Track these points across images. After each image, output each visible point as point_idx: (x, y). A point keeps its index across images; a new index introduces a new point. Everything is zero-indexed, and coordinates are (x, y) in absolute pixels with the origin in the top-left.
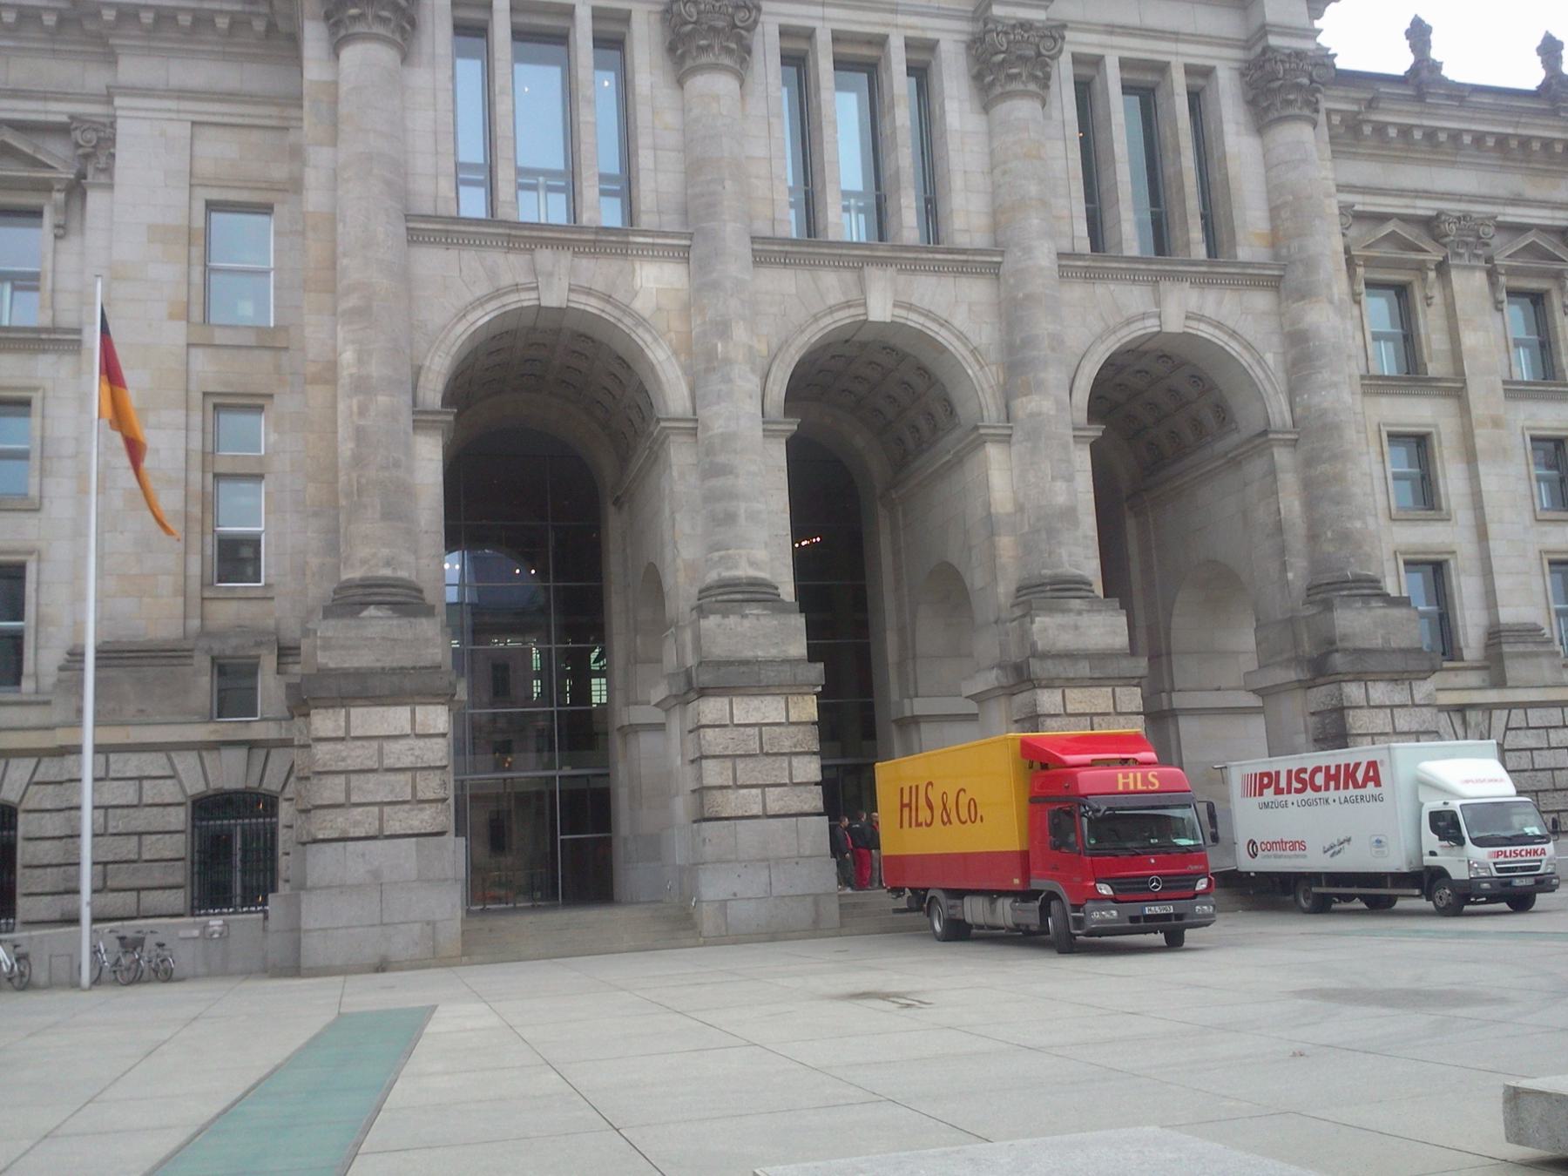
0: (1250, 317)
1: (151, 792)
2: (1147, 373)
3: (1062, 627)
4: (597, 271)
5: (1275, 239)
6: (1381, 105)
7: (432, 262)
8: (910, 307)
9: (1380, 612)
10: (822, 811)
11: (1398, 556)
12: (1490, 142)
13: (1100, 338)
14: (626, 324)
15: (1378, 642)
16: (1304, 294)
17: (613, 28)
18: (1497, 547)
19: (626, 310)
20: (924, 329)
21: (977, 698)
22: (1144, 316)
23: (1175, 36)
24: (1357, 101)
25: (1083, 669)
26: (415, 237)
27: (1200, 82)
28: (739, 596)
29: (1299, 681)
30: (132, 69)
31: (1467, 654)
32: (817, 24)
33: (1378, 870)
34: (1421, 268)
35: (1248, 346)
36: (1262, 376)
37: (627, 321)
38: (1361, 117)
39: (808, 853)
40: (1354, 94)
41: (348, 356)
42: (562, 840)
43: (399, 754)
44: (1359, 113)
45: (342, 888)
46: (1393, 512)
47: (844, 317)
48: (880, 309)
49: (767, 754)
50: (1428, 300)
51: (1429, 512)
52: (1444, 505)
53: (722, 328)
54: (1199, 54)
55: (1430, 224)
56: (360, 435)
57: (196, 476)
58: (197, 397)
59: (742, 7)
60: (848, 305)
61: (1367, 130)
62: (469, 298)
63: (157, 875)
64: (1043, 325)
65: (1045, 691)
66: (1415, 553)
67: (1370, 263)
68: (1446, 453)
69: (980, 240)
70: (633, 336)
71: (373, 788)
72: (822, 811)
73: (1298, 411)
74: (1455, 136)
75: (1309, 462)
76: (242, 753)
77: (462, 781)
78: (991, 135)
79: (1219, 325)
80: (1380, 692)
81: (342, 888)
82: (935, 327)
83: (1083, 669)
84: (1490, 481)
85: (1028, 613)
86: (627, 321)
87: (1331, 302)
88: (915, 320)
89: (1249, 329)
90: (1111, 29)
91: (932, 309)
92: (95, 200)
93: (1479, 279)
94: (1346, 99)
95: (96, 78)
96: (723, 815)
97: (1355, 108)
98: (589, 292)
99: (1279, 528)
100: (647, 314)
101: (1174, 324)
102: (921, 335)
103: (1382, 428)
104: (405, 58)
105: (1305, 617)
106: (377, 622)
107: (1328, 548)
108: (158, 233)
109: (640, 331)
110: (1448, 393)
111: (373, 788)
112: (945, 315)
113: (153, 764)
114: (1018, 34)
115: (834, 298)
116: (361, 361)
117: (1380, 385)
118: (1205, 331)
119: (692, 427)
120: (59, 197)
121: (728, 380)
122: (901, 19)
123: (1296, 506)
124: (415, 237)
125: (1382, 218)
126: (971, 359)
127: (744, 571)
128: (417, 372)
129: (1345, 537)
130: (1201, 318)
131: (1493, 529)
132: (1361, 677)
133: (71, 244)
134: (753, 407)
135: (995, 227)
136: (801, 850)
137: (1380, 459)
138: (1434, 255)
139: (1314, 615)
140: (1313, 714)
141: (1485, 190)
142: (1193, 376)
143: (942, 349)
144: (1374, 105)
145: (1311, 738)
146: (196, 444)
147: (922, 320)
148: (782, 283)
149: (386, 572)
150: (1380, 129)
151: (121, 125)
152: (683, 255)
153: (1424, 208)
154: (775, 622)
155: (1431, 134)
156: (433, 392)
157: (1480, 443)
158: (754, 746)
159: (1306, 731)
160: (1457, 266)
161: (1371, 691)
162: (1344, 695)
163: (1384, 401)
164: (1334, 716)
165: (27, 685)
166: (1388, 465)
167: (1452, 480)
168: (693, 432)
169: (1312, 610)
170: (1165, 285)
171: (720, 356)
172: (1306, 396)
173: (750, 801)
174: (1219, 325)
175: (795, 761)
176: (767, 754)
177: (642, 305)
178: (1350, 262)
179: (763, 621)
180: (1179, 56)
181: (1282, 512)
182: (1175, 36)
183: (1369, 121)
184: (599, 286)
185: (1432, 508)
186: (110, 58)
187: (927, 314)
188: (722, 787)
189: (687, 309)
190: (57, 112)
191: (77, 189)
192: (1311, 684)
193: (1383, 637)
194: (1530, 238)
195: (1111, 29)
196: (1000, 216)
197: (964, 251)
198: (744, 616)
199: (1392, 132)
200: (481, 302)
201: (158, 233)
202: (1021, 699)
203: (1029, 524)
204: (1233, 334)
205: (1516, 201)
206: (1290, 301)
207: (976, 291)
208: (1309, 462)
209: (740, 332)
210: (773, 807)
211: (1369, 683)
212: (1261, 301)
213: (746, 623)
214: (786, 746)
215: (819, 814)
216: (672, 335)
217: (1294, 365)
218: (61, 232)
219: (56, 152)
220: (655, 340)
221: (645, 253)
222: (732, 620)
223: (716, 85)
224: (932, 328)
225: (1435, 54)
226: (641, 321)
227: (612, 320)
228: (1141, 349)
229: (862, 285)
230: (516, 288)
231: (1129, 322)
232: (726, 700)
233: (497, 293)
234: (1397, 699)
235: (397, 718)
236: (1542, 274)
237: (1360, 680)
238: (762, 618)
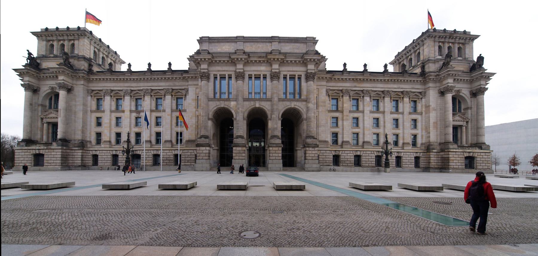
1: (192, 154)
3: (273, 141)
4: (227, 103)
5: (307, 96)
7: (211, 103)
8: (261, 105)
12: (351, 79)
13: (284, 108)
14: (230, 108)
15: (311, 143)
16: (309, 102)
17: (230, 76)
18: (345, 131)
19: (230, 107)
21: (301, 148)
22: (289, 105)
23: (297, 71)
26: (209, 101)
27: (300, 76)
30: (190, 83)
31: (339, 144)
32: (252, 74)
35: (302, 109)
40: (330, 74)
41: (201, 113)
43: (204, 152)
45: (199, 163)
47: (253, 107)
48: (257, 106)
50: (340, 100)
53: (239, 109)
54: (300, 73)
56: (202, 121)
57: (196, 124)
58: (196, 116)
59: (303, 55)
60: (254, 105)
63: (192, 161)
64: (275, 107)
67: (332, 96)
68: (340, 120)
69: (270, 97)
71: (202, 155)
74: (346, 79)
75: (307, 123)
76: (156, 151)
78: (272, 85)
79: (298, 106)
80: (311, 149)
81: (199, 163)
83: (275, 145)
84: (345, 123)
85: (306, 139)
87: (312, 103)
88: (261, 107)
89: (302, 107)
90: (288, 71)
92: (187, 96)
93: (348, 97)
94: (329, 75)
95: (187, 84)
98: (226, 105)
101: (293, 106)
104: (208, 82)
106: (203, 139)
107: (308, 132)
108: (193, 100)
110: (341, 112)
111: (202, 155)
113: (192, 151)
114: (275, 73)
115: (252, 105)
116: (202, 114)
118: (297, 107)
119: (236, 119)
120: (184, 96)
121: (239, 114)
122: (262, 72)
123: (306, 127)
124: (209, 101)
127: (239, 134)
128: (209, 114)
129: (310, 131)
130: (296, 105)
131: (344, 129)
132: (308, 147)
133: (185, 101)
134: (242, 117)
135: (272, 96)
138: (341, 95)
141: (350, 86)
146: (196, 121)
148: (247, 103)
149: (204, 134)
150: (335, 79)
151: (189, 89)
152: (236, 101)
153: (341, 88)
155: (342, 79)
156: (211, 116)
157: (344, 118)
160: (345, 96)
163: (332, 113)
165: (183, 143)
167: (340, 123)
168: (236, 119)
170: (291, 102)
173: (238, 158)
174: (298, 106)
177: (231, 106)
180: (297, 74)
182: (297, 71)
184: (227, 105)
186: (188, 81)
187: (263, 106)
189: (236, 107)
190: (183, 88)
191: (185, 96)
194: (356, 92)
195: (288, 71)
196: (272, 94)
199: (337, 79)
200: (215, 107)
201: (193, 100)
202: (305, 148)
204: (300, 107)
205: (356, 87)
207: (269, 103)
208: (307, 123)
209: (240, 109)
212: (304, 103)
214: (242, 152)
218: (185, 100)
219: (184, 92)
223: (240, 82)
224: (263, 108)
225: (347, 68)
226: (231, 108)
229: (255, 103)
230: (219, 105)
231: (287, 106)
233: (217, 106)
234: (313, 150)
235: (204, 148)
236: (358, 96)
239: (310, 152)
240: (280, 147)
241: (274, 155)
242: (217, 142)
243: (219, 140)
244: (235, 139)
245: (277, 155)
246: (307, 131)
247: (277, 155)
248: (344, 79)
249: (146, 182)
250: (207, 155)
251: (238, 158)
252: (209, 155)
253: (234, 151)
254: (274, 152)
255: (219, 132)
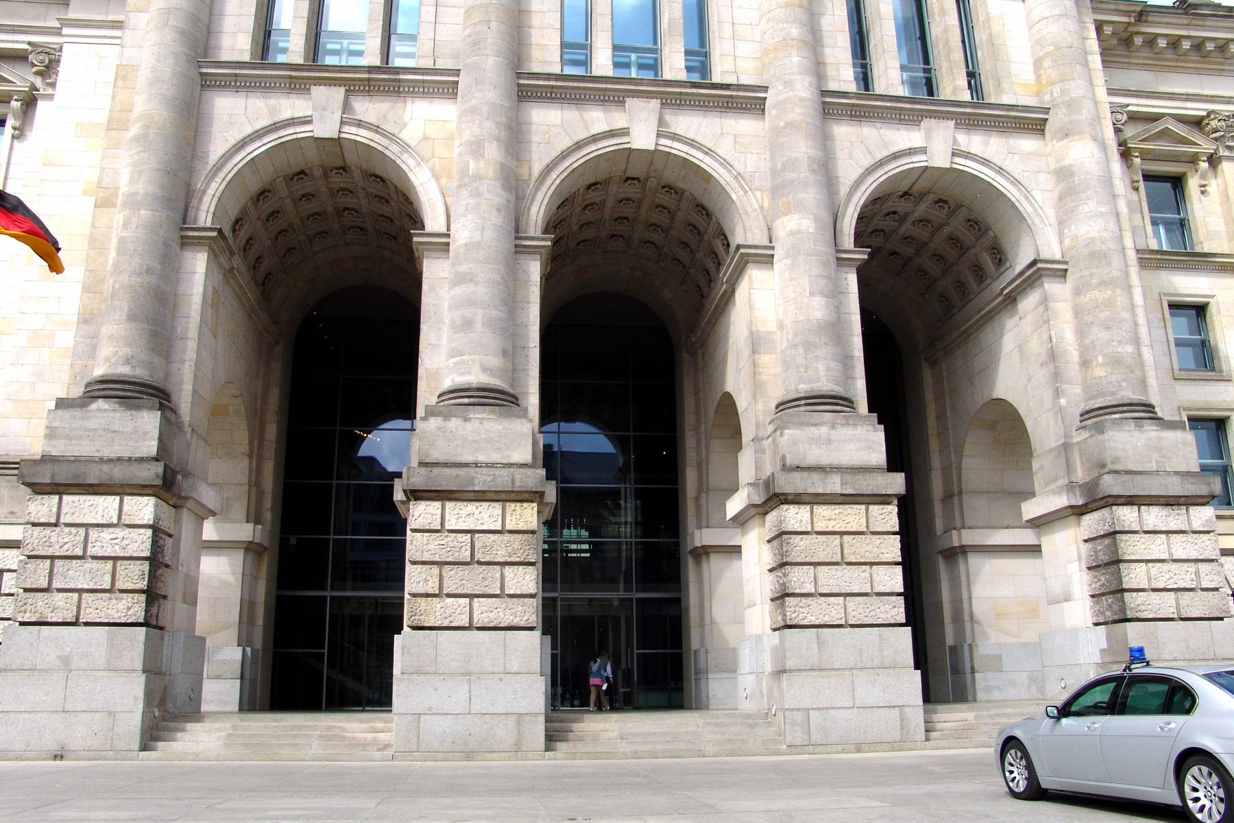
0: (1016, 157)
2: (928, 221)
3: (813, 440)
6: (1150, 19)
9: (1154, 434)
10: (904, 621)
11: (1182, 412)
14: (392, 151)
15: (1153, 466)
20: (688, 157)
24: (1127, 13)
25: (834, 485)
28: (466, 401)
29: (1071, 507)
33: (1078, 808)
34: (1193, 160)
36: (1030, 210)
37: (395, 148)
38: (1131, 29)
39: (515, 669)
42: (324, 649)
43: (103, 542)
44: (1129, 24)
46: (1177, 372)
48: (643, 138)
49: (479, 563)
51: (1210, 373)
52: (1224, 368)
55: (1197, 123)
61: (1138, 41)
62: (249, 130)
65: (791, 507)
66: (1198, 409)
70: (398, 162)
72: (904, 621)
73: (1067, 242)
77: (555, 599)
82: (699, 155)
86: (394, 148)
91: (697, 139)
96: (426, 625)
97: (1125, 19)
99: (1053, 356)
100: (413, 144)
102: (686, 164)
103: (1162, 297)
105: (1077, 443)
109: (405, 157)
112: (709, 145)
117: (1159, 259)
125: (1154, 118)
126: (734, 183)
136: (508, 666)
137: (1162, 324)
139: (1085, 439)
140: (1086, 541)
142: (969, 221)
143: (706, 177)
144: (1144, 18)
145: (1084, 566)
147: (686, 148)
150: (1151, 41)
153: (1196, 109)
154: (500, 427)
155: (1198, 46)
158: (465, 555)
159: (1080, 559)
161: (1145, 515)
162: (1116, 518)
164: (1107, 541)
166: (1170, 330)
169: (1085, 435)
171: (470, 174)
172: (1073, 227)
173: (454, 610)
175: (508, 570)
176: (479, 563)
178: (1126, 155)
179: (487, 425)
181: (1054, 340)
183: (1138, 33)
185: (1213, 369)
188: (427, 595)
192: (1083, 509)
193: (1157, 461)
197: (727, 87)
198: (466, 420)
203: (787, 340)
206: (1055, 141)
210: (480, 620)
211: (1142, 507)
213: (469, 427)
215: (901, 625)
216: (437, 161)
217: (1060, 199)
218: (19, 134)
220: (419, 164)
221: (416, 90)
222: (454, 423)
226: (405, 147)
227: (379, 148)
228: (915, 188)
232: (438, 504)
237: (1132, 504)
238: (485, 422)
239: (1156, 547)
240: (883, 499)
241: (831, 579)
242: (255, 483)
243: (272, 431)
244: (434, 423)
245: (855, 579)
246: (1085, 363)
247: (855, 579)
248: (1210, 46)
249: (1067, 270)
250: (135, 576)
251: (454, 610)
252: (153, 577)
253: (415, 545)
254: (826, 549)
255: (275, 399)
